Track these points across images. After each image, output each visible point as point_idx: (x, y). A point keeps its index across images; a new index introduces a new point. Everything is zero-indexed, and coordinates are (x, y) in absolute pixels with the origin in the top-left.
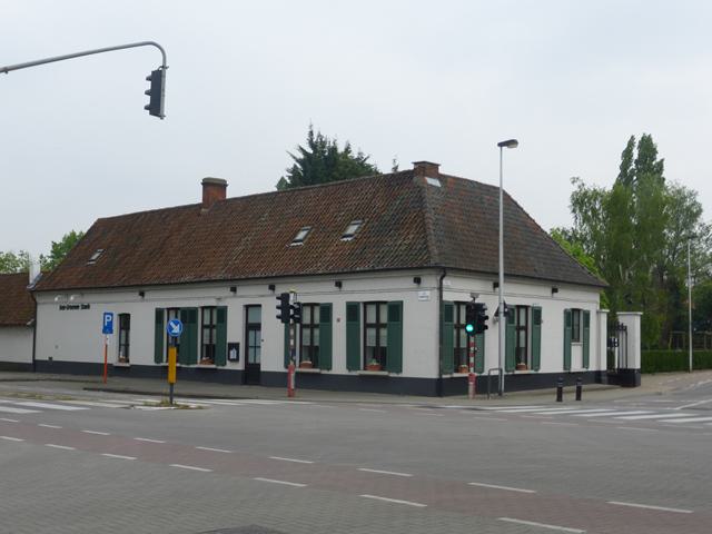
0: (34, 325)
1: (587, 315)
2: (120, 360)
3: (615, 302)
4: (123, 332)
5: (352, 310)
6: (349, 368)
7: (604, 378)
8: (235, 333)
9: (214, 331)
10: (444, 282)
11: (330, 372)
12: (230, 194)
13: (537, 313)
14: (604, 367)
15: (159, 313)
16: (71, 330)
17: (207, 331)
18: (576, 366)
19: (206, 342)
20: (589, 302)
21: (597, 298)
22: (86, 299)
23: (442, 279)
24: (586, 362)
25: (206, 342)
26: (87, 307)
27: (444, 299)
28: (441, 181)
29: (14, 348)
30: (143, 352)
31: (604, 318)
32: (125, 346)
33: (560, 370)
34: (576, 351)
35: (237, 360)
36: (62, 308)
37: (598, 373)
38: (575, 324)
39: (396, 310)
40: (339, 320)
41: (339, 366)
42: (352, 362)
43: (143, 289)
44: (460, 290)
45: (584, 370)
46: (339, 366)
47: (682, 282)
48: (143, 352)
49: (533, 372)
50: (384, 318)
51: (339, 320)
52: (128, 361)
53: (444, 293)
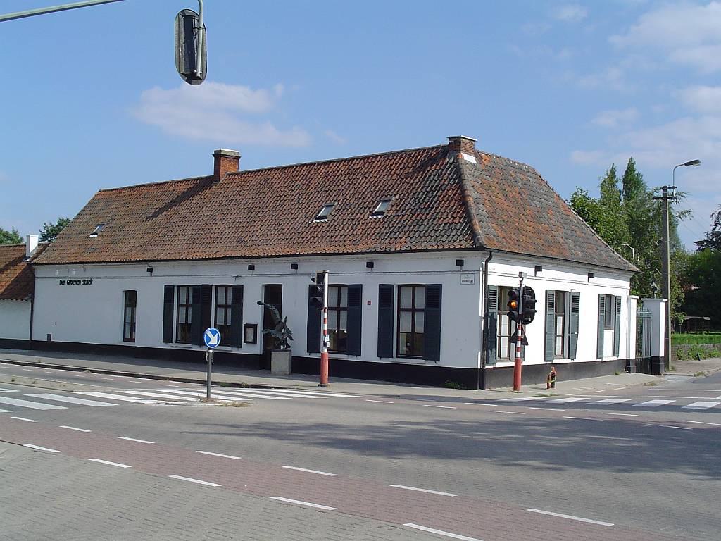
0: (33, 298)
1: (618, 300)
2: (125, 340)
3: (641, 287)
4: (129, 310)
5: (386, 293)
6: (380, 355)
7: (633, 366)
8: (252, 312)
9: (229, 311)
10: (490, 265)
11: (359, 359)
12: (242, 167)
13: (576, 298)
14: (633, 356)
15: (169, 290)
16: (79, 307)
17: (182, 310)
18: (608, 355)
19: (494, 349)
20: (620, 287)
21: (627, 284)
22: (89, 273)
23: (486, 263)
24: (616, 351)
25: (182, 321)
26: (90, 282)
27: (489, 283)
28: (476, 157)
29: (4, 321)
30: (150, 334)
31: (634, 303)
32: (130, 324)
33: (594, 359)
34: (608, 337)
35: (255, 342)
36: (63, 283)
37: (627, 362)
38: (608, 306)
39: (434, 294)
40: (369, 303)
41: (369, 352)
42: (384, 349)
43: (151, 264)
44: (503, 274)
45: (615, 358)
46: (369, 352)
47: (690, 256)
48: (150, 334)
49: (569, 361)
50: (421, 302)
51: (369, 303)
52: (133, 340)
53: (489, 277)
